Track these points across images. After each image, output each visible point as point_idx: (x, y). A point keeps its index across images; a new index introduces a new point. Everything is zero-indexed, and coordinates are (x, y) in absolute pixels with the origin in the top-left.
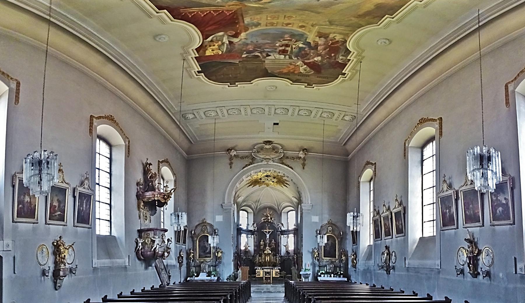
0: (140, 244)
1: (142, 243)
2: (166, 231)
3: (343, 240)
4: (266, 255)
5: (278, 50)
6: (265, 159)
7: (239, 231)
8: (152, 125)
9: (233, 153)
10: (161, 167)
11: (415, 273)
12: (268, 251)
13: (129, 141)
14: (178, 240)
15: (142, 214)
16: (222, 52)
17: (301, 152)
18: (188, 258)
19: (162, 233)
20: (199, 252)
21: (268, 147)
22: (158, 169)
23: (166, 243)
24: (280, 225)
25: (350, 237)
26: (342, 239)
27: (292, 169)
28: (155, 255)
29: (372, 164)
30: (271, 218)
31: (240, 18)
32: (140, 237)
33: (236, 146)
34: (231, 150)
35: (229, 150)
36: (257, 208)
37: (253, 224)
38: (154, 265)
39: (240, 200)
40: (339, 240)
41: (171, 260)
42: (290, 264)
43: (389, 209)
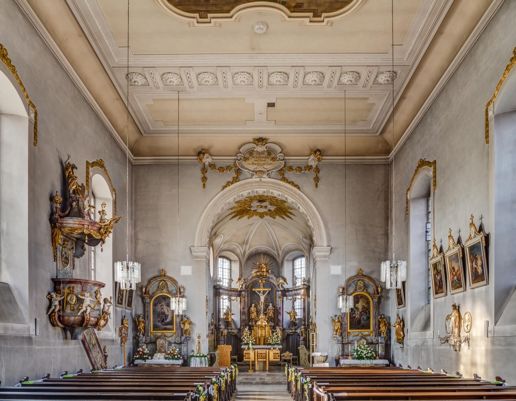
0: (57, 303)
1: (60, 302)
2: (102, 285)
3: (382, 300)
4: (261, 322)
6: (256, 172)
7: (217, 291)
9: (207, 160)
10: (91, 174)
11: (506, 345)
12: (262, 321)
13: (36, 113)
14: (119, 302)
15: (59, 254)
17: (312, 157)
18: (136, 328)
19: (96, 288)
20: (154, 322)
21: (260, 149)
22: (87, 176)
23: (102, 306)
24: (281, 281)
25: (393, 296)
26: (380, 299)
27: (299, 188)
28: (83, 323)
29: (429, 164)
30: (267, 271)
32: (56, 290)
33: (210, 147)
34: (204, 154)
35: (201, 153)
36: (244, 253)
37: (239, 279)
38: (80, 337)
39: (218, 241)
40: (376, 300)
41: (109, 332)
42: (296, 341)
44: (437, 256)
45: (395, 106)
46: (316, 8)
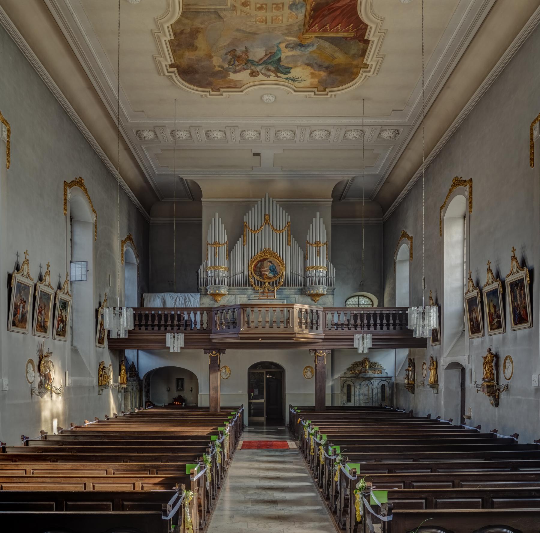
8: (65, 112)
13: (9, 131)
31: (307, 19)
43: (498, 275)
44: (493, 283)
45: (425, 114)
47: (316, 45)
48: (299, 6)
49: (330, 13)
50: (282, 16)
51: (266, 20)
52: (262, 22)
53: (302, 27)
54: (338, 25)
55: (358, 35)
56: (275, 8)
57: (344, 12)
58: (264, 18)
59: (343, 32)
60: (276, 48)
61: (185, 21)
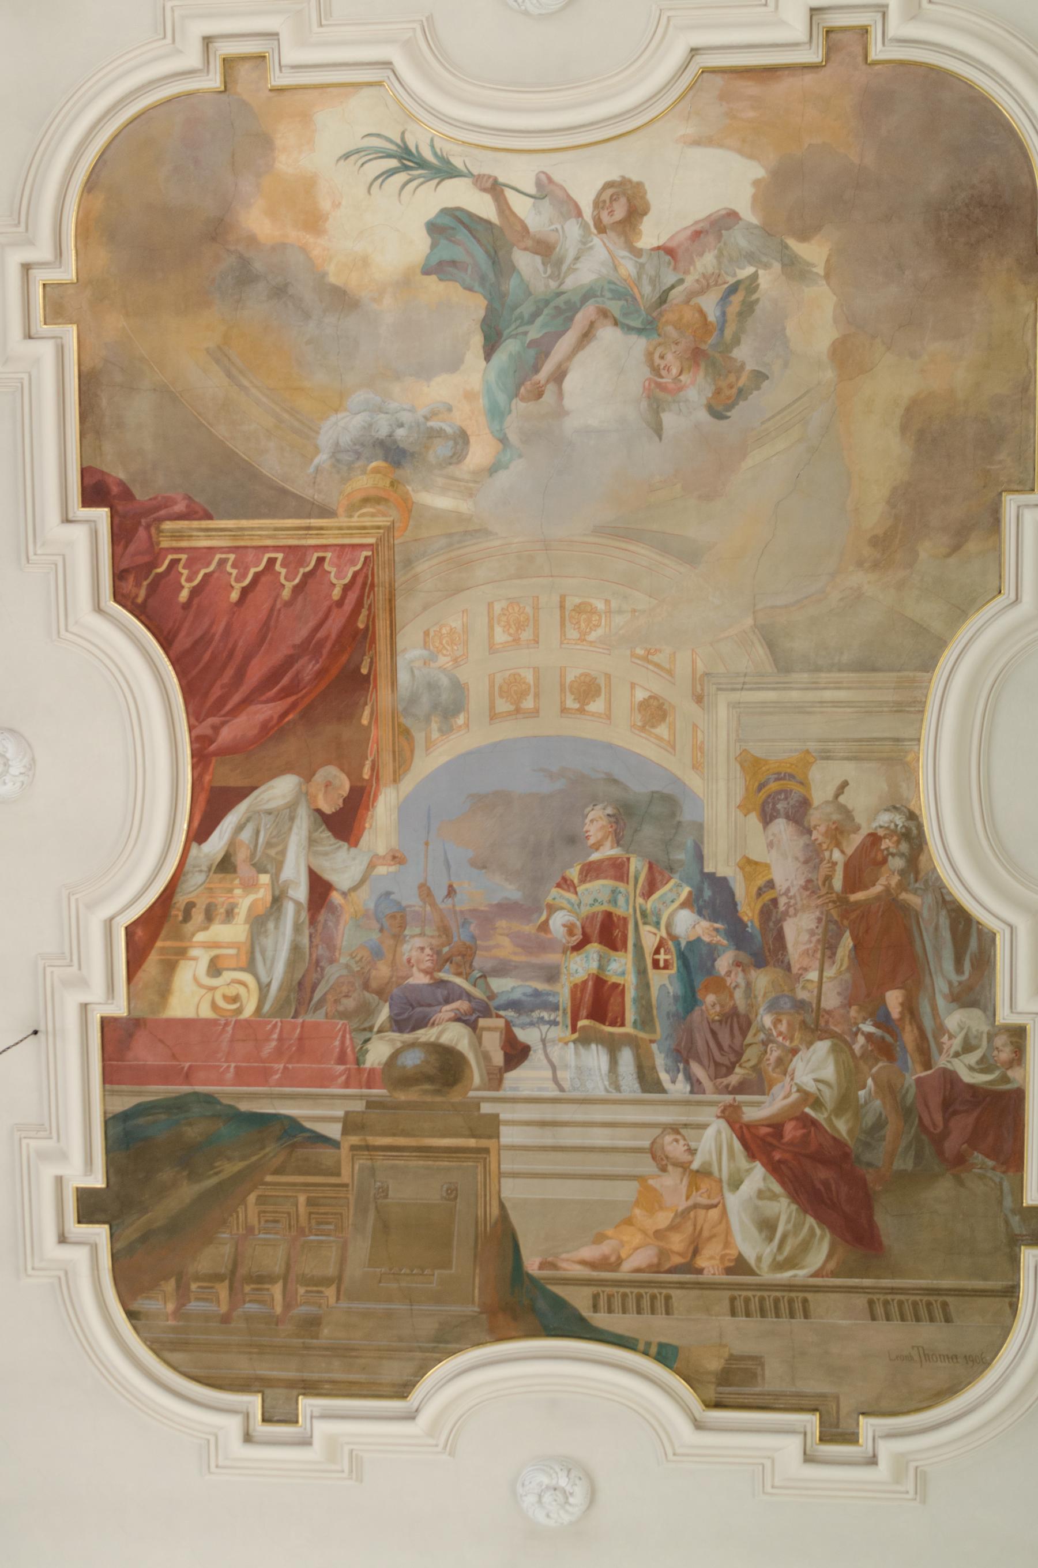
5: (563, 995)
16: (263, 989)
46: (825, 1388)
47: (323, 458)
48: (425, 700)
49: (289, 661)
50: (492, 649)
51: (563, 624)
52: (579, 609)
53: (400, 578)
54: (245, 592)
55: (142, 532)
56: (523, 694)
57: (230, 672)
58: (572, 634)
59: (212, 550)
60: (512, 427)
61: (927, 611)
